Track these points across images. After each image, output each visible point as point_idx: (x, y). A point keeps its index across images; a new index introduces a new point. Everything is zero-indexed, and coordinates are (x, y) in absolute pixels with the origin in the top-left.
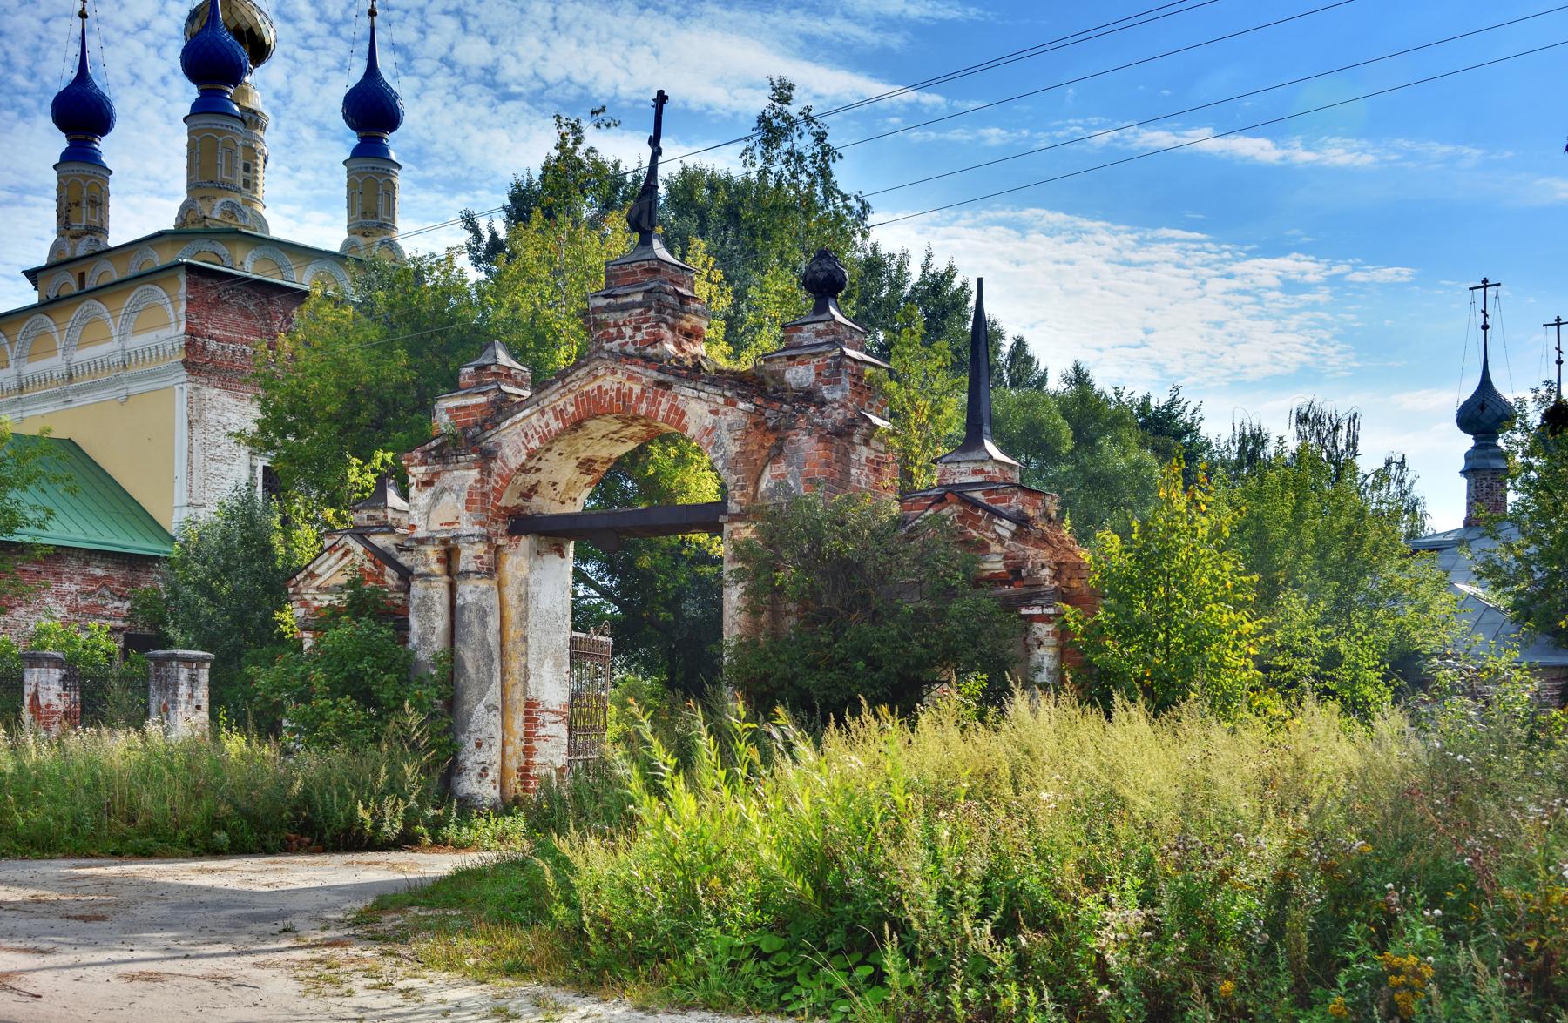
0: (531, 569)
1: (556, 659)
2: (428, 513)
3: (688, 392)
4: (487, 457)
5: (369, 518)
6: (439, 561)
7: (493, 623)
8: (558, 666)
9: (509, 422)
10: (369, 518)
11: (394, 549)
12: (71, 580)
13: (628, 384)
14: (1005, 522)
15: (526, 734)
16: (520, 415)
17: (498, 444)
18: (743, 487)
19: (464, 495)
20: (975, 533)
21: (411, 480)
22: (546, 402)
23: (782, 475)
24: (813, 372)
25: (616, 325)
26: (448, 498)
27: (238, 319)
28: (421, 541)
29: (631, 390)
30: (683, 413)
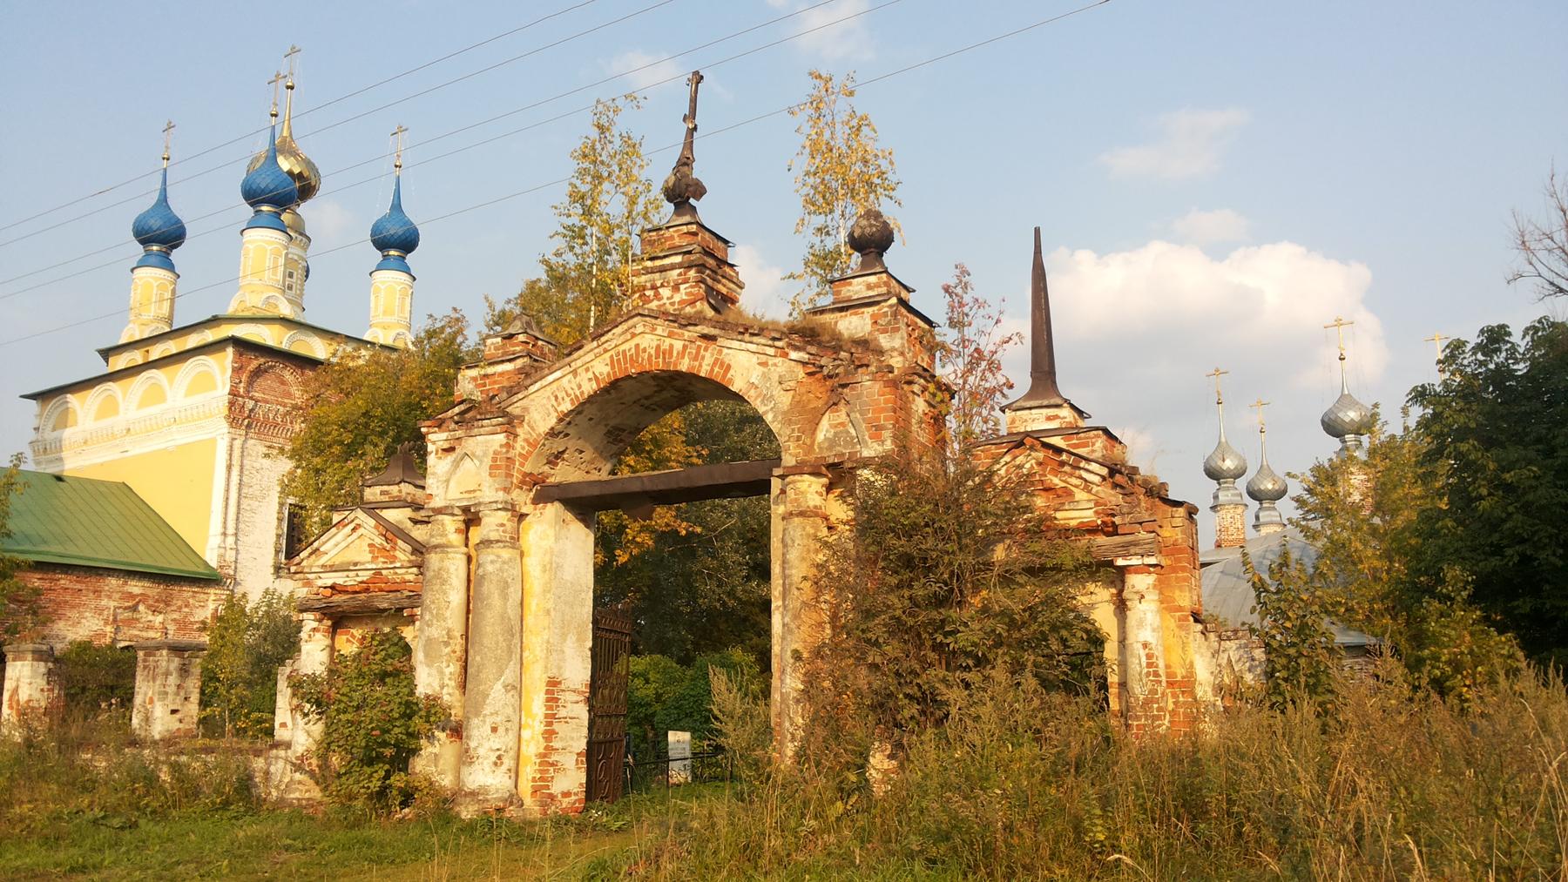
0: (557, 539)
1: (579, 634)
2: (448, 481)
3: (736, 344)
4: (510, 424)
5: (382, 493)
6: (458, 531)
7: (514, 596)
8: (580, 640)
9: (538, 385)
10: (382, 493)
11: (409, 524)
12: (110, 597)
13: (668, 341)
14: (1094, 467)
15: (547, 716)
16: (550, 378)
17: (525, 409)
18: (798, 439)
19: (488, 461)
20: (1056, 481)
21: (430, 447)
22: (579, 363)
23: (842, 424)
24: (869, 321)
25: (654, 288)
27: (275, 385)
28: (439, 511)
29: (671, 346)
30: (729, 367)
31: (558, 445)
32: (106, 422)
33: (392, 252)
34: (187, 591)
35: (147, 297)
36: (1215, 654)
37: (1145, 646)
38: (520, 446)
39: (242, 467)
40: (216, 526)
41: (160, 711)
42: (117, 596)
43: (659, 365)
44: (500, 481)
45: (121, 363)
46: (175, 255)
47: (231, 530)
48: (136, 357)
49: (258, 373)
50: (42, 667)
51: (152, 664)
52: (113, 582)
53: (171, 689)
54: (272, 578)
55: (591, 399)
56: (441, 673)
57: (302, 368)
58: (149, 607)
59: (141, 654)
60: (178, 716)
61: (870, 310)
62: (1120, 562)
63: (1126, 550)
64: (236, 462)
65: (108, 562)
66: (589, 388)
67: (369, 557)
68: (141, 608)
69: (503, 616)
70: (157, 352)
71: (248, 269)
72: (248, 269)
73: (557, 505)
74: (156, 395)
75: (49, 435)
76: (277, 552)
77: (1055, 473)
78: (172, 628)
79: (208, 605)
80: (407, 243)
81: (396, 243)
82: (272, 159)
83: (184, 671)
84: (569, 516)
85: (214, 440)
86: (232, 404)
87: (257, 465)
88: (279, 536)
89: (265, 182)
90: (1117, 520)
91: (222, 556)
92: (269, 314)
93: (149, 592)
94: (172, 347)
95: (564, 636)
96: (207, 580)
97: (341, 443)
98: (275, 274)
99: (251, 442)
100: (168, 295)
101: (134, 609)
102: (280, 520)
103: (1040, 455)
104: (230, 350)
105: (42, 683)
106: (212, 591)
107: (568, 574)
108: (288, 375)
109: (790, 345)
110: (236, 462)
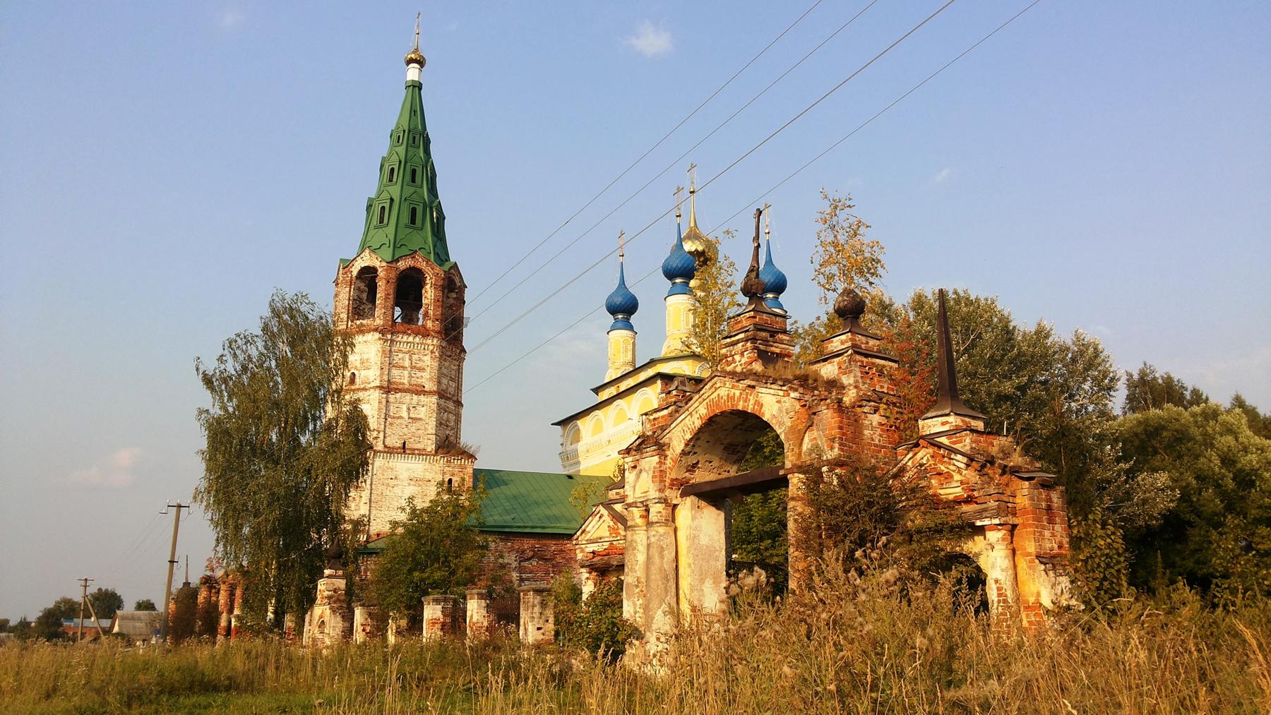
0: (694, 518)
3: (764, 390)
4: (661, 448)
7: (669, 555)
14: (959, 457)
19: (651, 473)
26: (644, 475)
31: (692, 460)
35: (617, 349)
36: (1053, 586)
37: (996, 581)
38: (669, 462)
41: (531, 628)
43: (728, 407)
44: (657, 486)
48: (611, 391)
50: (483, 603)
53: (536, 615)
55: (700, 430)
56: (635, 605)
61: (837, 360)
62: (978, 523)
63: (981, 514)
66: (698, 423)
67: (608, 534)
69: (661, 569)
70: (624, 386)
73: (692, 497)
75: (569, 448)
77: (942, 463)
82: (680, 245)
83: (543, 605)
84: (703, 504)
89: (676, 263)
90: (976, 494)
94: (631, 382)
95: (702, 581)
100: (630, 347)
103: (931, 450)
104: (659, 382)
105: (484, 612)
107: (704, 540)
109: (791, 388)
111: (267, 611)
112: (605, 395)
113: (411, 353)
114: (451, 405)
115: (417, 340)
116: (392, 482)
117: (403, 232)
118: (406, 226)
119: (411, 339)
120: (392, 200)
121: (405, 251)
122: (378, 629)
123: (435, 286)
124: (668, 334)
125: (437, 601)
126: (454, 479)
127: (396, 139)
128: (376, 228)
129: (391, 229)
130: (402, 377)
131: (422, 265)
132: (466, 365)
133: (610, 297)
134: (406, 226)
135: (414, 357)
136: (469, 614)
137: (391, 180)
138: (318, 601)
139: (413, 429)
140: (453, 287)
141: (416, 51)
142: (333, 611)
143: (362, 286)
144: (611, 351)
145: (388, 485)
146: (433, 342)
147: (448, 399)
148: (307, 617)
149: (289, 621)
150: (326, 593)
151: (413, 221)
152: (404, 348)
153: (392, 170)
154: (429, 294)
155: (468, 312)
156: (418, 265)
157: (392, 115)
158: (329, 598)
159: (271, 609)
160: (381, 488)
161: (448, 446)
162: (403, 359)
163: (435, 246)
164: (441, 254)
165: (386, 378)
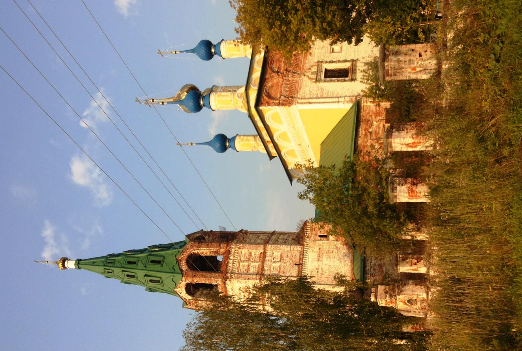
27: (274, 89)
32: (297, 153)
33: (213, 50)
34: (363, 114)
35: (246, 145)
39: (309, 98)
40: (335, 106)
42: (366, 139)
45: (274, 152)
46: (229, 136)
47: (337, 100)
48: (270, 146)
49: (269, 96)
50: (396, 134)
51: (393, 71)
52: (360, 142)
53: (407, 58)
54: (356, 82)
57: (265, 79)
58: (370, 127)
59: (387, 78)
60: (423, 53)
64: (307, 101)
65: (352, 144)
68: (370, 130)
70: (267, 138)
71: (227, 106)
72: (227, 106)
74: (284, 136)
76: (345, 81)
78: (379, 118)
79: (368, 105)
80: (208, 44)
81: (208, 50)
83: (397, 53)
85: (300, 111)
86: (283, 105)
87: (308, 92)
88: (338, 81)
89: (191, 104)
91: (348, 102)
92: (245, 96)
93: (364, 128)
94: (264, 133)
96: (358, 106)
97: (280, 26)
98: (228, 96)
99: (299, 96)
100: (245, 138)
101: (371, 133)
102: (331, 81)
104: (261, 108)
105: (403, 133)
106: (362, 105)
108: (269, 84)
110: (307, 101)
111: (400, 345)
112: (273, 152)
113: (240, 261)
114: (274, 237)
115: (231, 257)
116: (320, 272)
117: (165, 268)
118: (162, 266)
119: (231, 261)
120: (146, 275)
121: (176, 267)
122: (417, 250)
123: (198, 247)
124: (234, 108)
125: (394, 189)
126: (319, 234)
127: (109, 274)
128: (163, 285)
129: (164, 276)
130: (254, 267)
131: (185, 255)
132: (250, 229)
133: (216, 150)
134: (162, 266)
135: (242, 259)
136: (404, 149)
137: (134, 277)
138: (393, 305)
139: (287, 259)
140: (200, 238)
141: (57, 263)
142: (401, 292)
143: (198, 293)
144: (248, 149)
145: (322, 274)
146: (234, 248)
147: (269, 239)
148: (405, 314)
149: (407, 329)
150: (388, 299)
151: (158, 262)
152: (236, 265)
153: (128, 276)
154: (204, 251)
155: (217, 229)
156: (185, 258)
157: (95, 278)
158: (391, 296)
159: (399, 342)
160: (323, 279)
161: (299, 238)
162: (244, 266)
163: (175, 248)
164: (182, 245)
165: (254, 276)
